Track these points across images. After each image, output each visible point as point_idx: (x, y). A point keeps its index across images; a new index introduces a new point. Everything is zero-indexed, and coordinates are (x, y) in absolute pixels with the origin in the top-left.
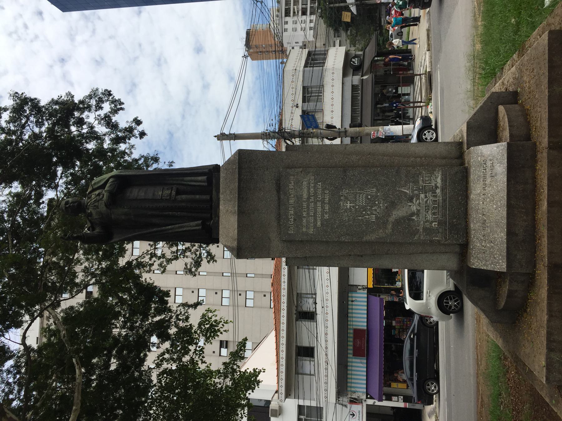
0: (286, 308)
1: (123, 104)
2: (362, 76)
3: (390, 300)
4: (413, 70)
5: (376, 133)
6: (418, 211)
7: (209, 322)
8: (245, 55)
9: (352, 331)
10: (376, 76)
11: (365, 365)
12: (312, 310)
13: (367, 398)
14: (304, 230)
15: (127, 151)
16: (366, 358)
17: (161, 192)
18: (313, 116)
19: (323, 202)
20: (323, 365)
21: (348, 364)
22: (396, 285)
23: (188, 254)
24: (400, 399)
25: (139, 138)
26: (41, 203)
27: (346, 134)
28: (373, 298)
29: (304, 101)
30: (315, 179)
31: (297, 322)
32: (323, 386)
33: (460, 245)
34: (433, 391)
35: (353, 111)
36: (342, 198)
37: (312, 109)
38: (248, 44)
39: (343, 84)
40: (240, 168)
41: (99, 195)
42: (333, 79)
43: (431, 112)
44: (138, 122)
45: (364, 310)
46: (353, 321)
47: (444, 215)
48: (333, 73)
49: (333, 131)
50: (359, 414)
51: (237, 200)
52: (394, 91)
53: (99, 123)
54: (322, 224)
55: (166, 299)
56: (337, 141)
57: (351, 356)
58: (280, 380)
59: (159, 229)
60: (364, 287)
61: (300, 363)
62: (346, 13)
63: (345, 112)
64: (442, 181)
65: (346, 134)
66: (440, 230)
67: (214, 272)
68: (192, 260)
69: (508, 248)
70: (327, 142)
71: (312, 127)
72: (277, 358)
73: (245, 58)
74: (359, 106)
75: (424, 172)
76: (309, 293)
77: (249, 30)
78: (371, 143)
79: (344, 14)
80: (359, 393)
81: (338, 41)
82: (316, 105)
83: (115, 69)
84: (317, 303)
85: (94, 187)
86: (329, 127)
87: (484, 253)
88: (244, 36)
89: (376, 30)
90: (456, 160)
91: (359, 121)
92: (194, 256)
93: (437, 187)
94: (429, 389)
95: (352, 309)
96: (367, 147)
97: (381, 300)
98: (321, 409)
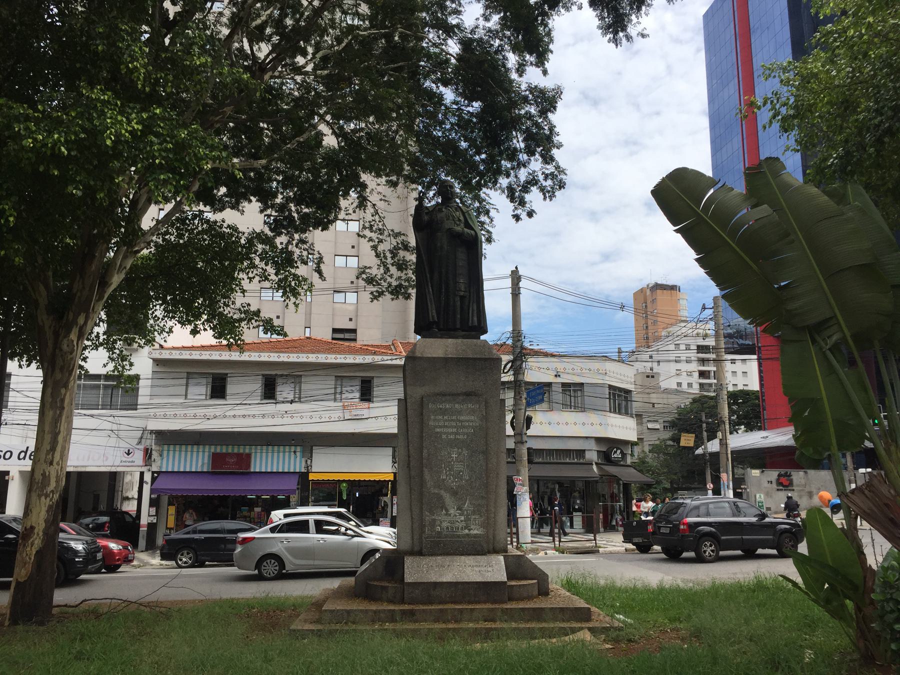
0: (281, 360)
1: (551, 200)
2: (596, 464)
4: (605, 532)
6: (450, 515)
7: (298, 286)
9: (247, 451)
10: (597, 482)
11: (199, 470)
12: (279, 398)
13: (153, 473)
14: (432, 417)
15: (498, 185)
16: (210, 470)
17: (462, 281)
18: (542, 401)
19: (456, 434)
20: (201, 412)
21: (201, 447)
23: (382, 270)
24: (152, 518)
27: (518, 442)
29: (564, 385)
31: (261, 377)
32: (170, 412)
33: (421, 550)
34: (181, 560)
35: (550, 452)
36: (460, 450)
37: (554, 397)
38: (658, 287)
39: (587, 438)
40: (486, 360)
41: (459, 220)
44: (530, 214)
45: (283, 468)
46: (261, 453)
47: (446, 536)
48: (601, 424)
50: (129, 462)
52: (577, 507)
55: (320, 228)
56: (509, 431)
57: (213, 450)
58: (169, 351)
59: (429, 280)
61: (204, 381)
62: (693, 439)
63: (550, 441)
65: (518, 442)
68: (374, 274)
70: (509, 417)
74: (557, 459)
78: (508, 477)
80: (159, 462)
83: (619, 74)
88: (670, 283)
89: (671, 483)
90: (492, 547)
91: (536, 460)
93: (469, 530)
94: (182, 555)
95: (284, 452)
96: (504, 471)
97: (293, 492)
98: (134, 406)
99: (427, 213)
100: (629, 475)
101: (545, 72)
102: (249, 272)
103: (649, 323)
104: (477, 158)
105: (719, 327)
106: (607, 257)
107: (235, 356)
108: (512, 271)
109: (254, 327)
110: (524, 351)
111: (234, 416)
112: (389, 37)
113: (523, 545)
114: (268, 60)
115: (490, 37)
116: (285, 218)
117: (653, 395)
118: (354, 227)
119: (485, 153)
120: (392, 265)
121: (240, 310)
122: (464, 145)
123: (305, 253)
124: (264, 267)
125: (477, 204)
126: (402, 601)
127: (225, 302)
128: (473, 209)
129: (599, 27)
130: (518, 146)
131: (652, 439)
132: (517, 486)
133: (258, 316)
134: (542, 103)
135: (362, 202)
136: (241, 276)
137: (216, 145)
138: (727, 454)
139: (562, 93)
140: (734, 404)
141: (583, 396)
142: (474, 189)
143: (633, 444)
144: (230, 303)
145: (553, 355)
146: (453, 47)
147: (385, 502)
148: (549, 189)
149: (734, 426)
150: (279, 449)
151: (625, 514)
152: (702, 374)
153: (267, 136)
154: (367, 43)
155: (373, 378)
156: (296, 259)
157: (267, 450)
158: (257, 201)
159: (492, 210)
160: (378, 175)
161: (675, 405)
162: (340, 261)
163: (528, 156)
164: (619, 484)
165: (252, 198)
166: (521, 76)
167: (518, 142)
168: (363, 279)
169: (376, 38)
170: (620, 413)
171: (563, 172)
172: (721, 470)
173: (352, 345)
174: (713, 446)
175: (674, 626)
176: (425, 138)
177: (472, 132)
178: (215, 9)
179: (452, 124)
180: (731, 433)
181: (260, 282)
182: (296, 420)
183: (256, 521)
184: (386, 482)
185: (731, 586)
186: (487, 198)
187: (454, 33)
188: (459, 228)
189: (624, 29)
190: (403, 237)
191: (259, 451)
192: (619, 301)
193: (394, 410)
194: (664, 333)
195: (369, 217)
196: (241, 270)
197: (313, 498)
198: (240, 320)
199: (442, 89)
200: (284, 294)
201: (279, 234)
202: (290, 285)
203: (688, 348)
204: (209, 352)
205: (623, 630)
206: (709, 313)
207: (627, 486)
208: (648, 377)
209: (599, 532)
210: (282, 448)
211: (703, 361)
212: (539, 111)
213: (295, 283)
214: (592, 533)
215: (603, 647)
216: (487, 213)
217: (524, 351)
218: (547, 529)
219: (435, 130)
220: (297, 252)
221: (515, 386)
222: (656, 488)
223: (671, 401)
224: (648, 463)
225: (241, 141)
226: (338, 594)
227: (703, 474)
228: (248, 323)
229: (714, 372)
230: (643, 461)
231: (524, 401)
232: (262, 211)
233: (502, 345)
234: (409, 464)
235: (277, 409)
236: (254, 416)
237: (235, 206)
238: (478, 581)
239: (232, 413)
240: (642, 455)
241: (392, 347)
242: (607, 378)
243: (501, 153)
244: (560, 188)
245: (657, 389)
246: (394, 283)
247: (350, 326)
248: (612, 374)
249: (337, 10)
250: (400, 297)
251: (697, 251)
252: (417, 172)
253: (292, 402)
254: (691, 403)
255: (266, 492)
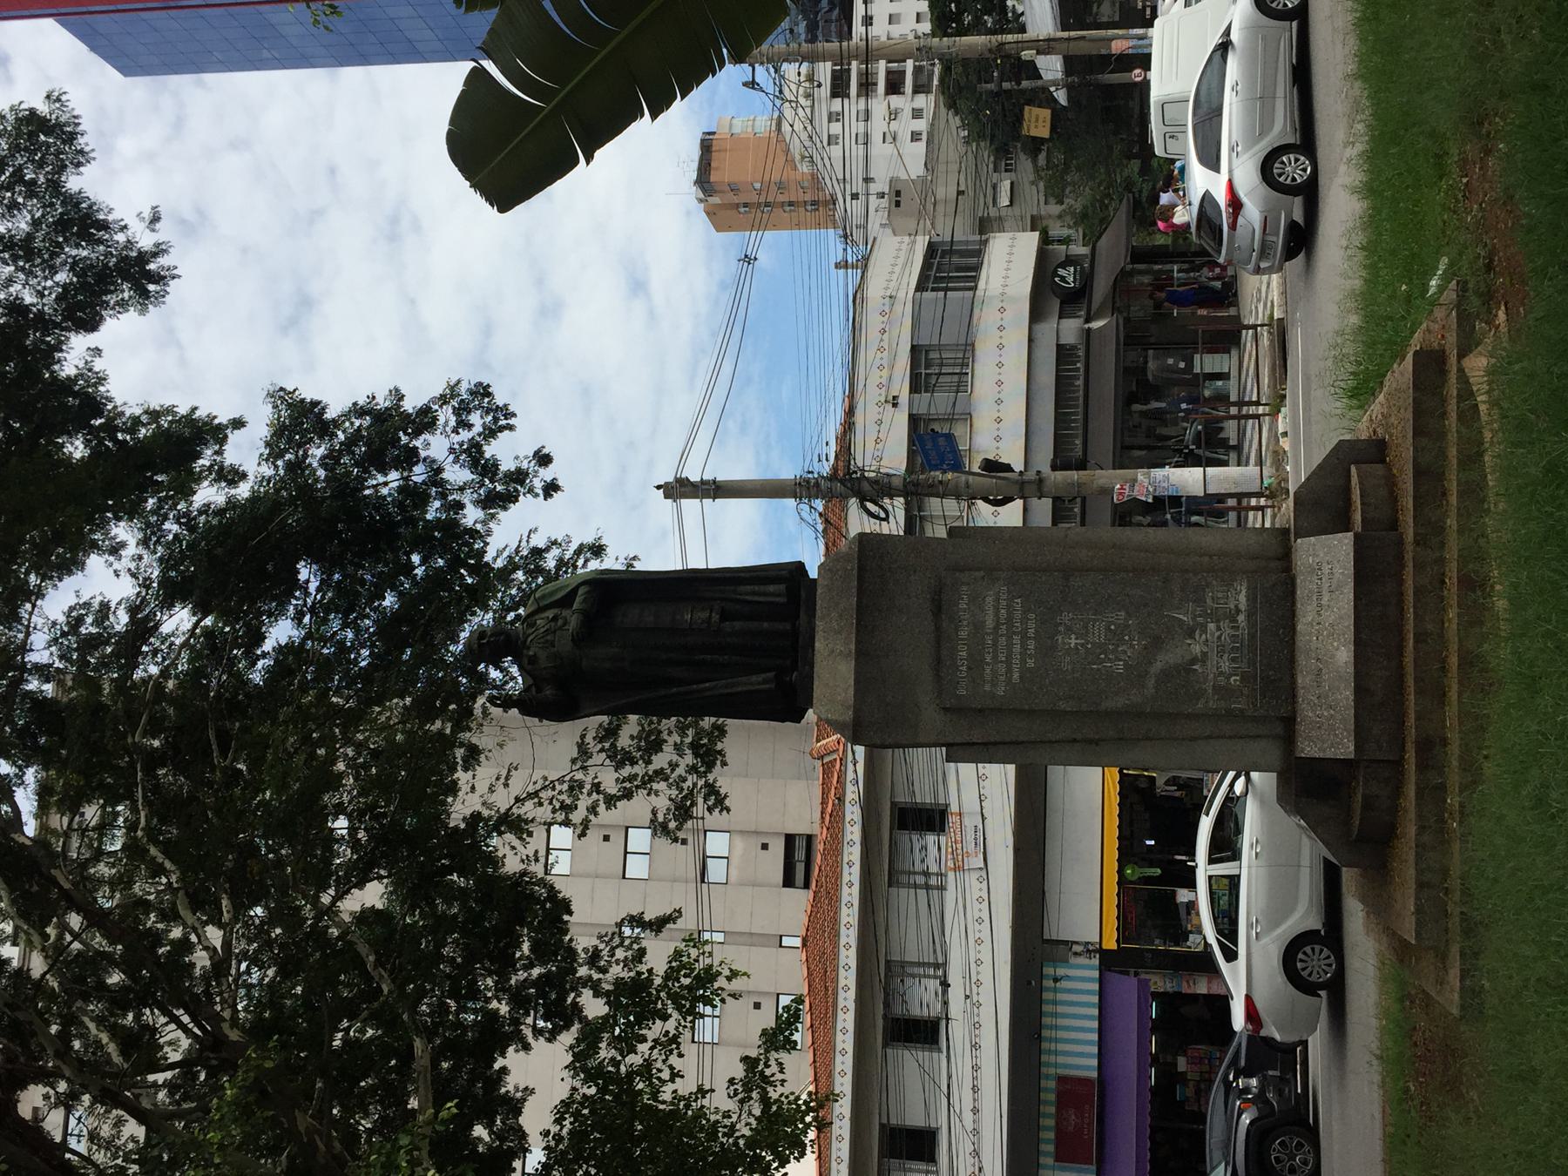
0: (852, 1006)
1: (514, 415)
2: (1087, 321)
3: (1170, 990)
5: (1127, 487)
8: (746, 256)
9: (1052, 1084)
10: (1127, 320)
12: (936, 1009)
14: (987, 688)
15: (479, 527)
16: (1094, 1168)
18: (950, 438)
22: (1188, 943)
23: (660, 786)
25: (542, 496)
26: (258, 658)
28: (1114, 978)
29: (915, 388)
30: (1009, 592)
31: (889, 1051)
33: (1283, 719)
35: (1061, 420)
36: (1061, 628)
37: (941, 410)
38: (704, 180)
39: (1030, 340)
40: (861, 569)
41: (555, 619)
42: (1001, 328)
43: (1285, 434)
44: (544, 459)
46: (1057, 1040)
47: (1252, 663)
48: (1002, 310)
49: (1000, 478)
51: (854, 631)
53: (456, 461)
54: (1021, 677)
55: (566, 917)
57: (1050, 1161)
59: (682, 689)
60: (1091, 948)
62: (1036, 111)
64: (1248, 600)
66: (1246, 691)
67: (591, 924)
68: (669, 803)
69: (1356, 716)
71: (945, 467)
72: (820, 1167)
73: (746, 264)
75: (1214, 582)
76: (926, 961)
77: (709, 134)
79: (1030, 113)
81: (1006, 185)
82: (954, 403)
84: (949, 985)
85: (541, 604)
86: (992, 466)
87: (1319, 727)
88: (695, 153)
89: (1130, 157)
91: (1079, 451)
92: (674, 792)
93: (1238, 611)
97: (1143, 985)
99: (539, 690)
100: (1113, 249)
101: (238, 424)
102: (659, 1079)
103: (781, 198)
104: (419, 572)
105: (793, 53)
106: (638, 286)
107: (843, 1109)
108: (666, 497)
109: (781, 1071)
110: (841, 474)
111: (975, 1111)
112: (153, 760)
113: (1266, 483)
114: (196, 1030)
115: (158, 542)
116: (542, 994)
117: (941, 193)
118: (562, 836)
119: (408, 554)
120: (649, 762)
121: (742, 1102)
122: (389, 600)
123: (620, 954)
124: (650, 1044)
125: (520, 575)
126: (1399, 763)
127: (725, 1135)
128: (529, 584)
129: (143, 311)
130: (396, 484)
131: (1033, 198)
132: (1135, 493)
133: (757, 1060)
134: (303, 433)
135: (513, 824)
136: (666, 1096)
137: (383, 1159)
138: (1069, 39)
139: (282, 389)
140: (959, 21)
141: (940, 348)
142: (489, 580)
143: (1045, 240)
144: (727, 1122)
145: (850, 412)
146: (179, 621)
147: (1167, 784)
148: (490, 418)
149: (1008, 21)
150: (1048, 1002)
151: (1198, 260)
152: (894, 87)
153: (362, 1031)
154: (164, 806)
155: (893, 804)
156: (632, 974)
157: (1050, 1040)
158: (503, 1055)
159: (533, 543)
160: (453, 789)
161: (962, 149)
162: (637, 867)
163: (417, 463)
164: (1132, 273)
165: (497, 1066)
166: (244, 476)
167: (386, 484)
168: (679, 828)
169: (156, 788)
170: (977, 268)
171: (453, 389)
172: (1103, 52)
173: (821, 847)
174: (1051, 67)
175: (1455, 170)
176: (375, 685)
177: (362, 582)
178: (82, 1148)
179: (344, 626)
180: (1023, 29)
181: (681, 1055)
182: (986, 977)
183: (1206, 1068)
184: (1124, 780)
185: (1362, 40)
186: (506, 554)
187: (147, 618)
188: (574, 621)
189: (144, 257)
190: (589, 739)
191: (1052, 1058)
192: (734, 266)
193: (967, 770)
194: (805, 168)
195: (544, 813)
196: (655, 1095)
197: (1157, 941)
198: (765, 1101)
199: (268, 646)
200: (708, 1002)
201: (577, 1009)
202: (689, 988)
203: (833, 117)
204: (834, 1164)
205: (1466, 282)
206: (763, 74)
207: (1138, 255)
208: (898, 204)
209: (1238, 318)
210: (1046, 1008)
211: (867, 87)
212: (321, 438)
213: (685, 976)
214: (1240, 332)
215: (1503, 329)
216: (538, 553)
217: (841, 474)
218: (1230, 430)
219: (356, 661)
220: (616, 971)
221: (917, 494)
222: (1141, 192)
223: (953, 156)
224: (1085, 207)
225: (372, 1090)
226: (1379, 908)
227: (1110, 90)
228: (772, 1084)
229: (889, 62)
230: (1082, 218)
231: (949, 476)
232: (527, 1047)
233: (827, 521)
234: (1090, 742)
235: (960, 1017)
236: (976, 1068)
237: (514, 1106)
238: (1352, 596)
239: (968, 1117)
240: (1069, 220)
241: (826, 760)
242: (901, 295)
243: (412, 522)
244: (489, 394)
245: (925, 186)
246: (689, 759)
247: (778, 847)
248: (892, 284)
249: (92, 871)
250: (719, 746)
251: (634, 114)
252: (446, 703)
253: (945, 985)
254: (956, 113)
255: (1142, 1044)
